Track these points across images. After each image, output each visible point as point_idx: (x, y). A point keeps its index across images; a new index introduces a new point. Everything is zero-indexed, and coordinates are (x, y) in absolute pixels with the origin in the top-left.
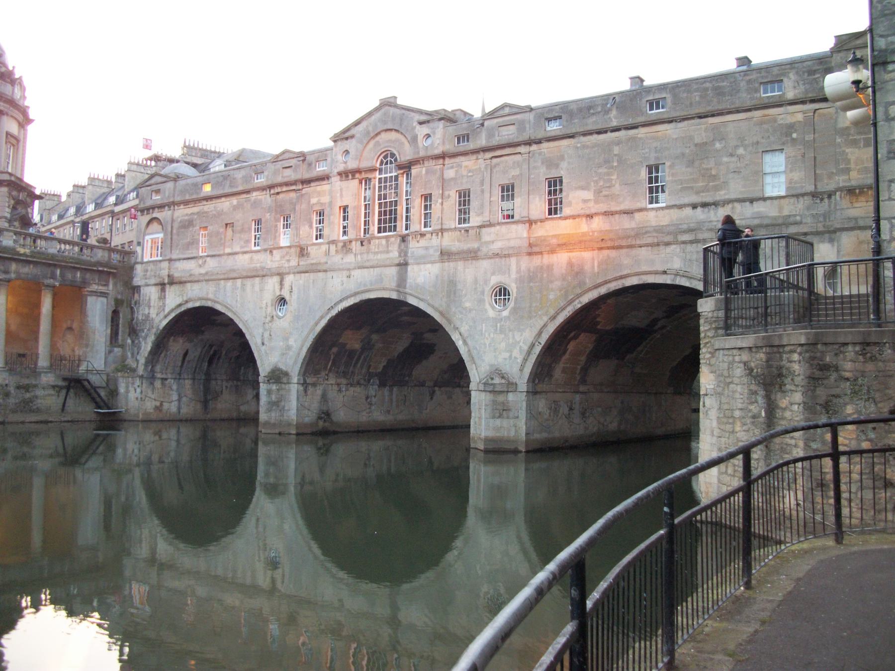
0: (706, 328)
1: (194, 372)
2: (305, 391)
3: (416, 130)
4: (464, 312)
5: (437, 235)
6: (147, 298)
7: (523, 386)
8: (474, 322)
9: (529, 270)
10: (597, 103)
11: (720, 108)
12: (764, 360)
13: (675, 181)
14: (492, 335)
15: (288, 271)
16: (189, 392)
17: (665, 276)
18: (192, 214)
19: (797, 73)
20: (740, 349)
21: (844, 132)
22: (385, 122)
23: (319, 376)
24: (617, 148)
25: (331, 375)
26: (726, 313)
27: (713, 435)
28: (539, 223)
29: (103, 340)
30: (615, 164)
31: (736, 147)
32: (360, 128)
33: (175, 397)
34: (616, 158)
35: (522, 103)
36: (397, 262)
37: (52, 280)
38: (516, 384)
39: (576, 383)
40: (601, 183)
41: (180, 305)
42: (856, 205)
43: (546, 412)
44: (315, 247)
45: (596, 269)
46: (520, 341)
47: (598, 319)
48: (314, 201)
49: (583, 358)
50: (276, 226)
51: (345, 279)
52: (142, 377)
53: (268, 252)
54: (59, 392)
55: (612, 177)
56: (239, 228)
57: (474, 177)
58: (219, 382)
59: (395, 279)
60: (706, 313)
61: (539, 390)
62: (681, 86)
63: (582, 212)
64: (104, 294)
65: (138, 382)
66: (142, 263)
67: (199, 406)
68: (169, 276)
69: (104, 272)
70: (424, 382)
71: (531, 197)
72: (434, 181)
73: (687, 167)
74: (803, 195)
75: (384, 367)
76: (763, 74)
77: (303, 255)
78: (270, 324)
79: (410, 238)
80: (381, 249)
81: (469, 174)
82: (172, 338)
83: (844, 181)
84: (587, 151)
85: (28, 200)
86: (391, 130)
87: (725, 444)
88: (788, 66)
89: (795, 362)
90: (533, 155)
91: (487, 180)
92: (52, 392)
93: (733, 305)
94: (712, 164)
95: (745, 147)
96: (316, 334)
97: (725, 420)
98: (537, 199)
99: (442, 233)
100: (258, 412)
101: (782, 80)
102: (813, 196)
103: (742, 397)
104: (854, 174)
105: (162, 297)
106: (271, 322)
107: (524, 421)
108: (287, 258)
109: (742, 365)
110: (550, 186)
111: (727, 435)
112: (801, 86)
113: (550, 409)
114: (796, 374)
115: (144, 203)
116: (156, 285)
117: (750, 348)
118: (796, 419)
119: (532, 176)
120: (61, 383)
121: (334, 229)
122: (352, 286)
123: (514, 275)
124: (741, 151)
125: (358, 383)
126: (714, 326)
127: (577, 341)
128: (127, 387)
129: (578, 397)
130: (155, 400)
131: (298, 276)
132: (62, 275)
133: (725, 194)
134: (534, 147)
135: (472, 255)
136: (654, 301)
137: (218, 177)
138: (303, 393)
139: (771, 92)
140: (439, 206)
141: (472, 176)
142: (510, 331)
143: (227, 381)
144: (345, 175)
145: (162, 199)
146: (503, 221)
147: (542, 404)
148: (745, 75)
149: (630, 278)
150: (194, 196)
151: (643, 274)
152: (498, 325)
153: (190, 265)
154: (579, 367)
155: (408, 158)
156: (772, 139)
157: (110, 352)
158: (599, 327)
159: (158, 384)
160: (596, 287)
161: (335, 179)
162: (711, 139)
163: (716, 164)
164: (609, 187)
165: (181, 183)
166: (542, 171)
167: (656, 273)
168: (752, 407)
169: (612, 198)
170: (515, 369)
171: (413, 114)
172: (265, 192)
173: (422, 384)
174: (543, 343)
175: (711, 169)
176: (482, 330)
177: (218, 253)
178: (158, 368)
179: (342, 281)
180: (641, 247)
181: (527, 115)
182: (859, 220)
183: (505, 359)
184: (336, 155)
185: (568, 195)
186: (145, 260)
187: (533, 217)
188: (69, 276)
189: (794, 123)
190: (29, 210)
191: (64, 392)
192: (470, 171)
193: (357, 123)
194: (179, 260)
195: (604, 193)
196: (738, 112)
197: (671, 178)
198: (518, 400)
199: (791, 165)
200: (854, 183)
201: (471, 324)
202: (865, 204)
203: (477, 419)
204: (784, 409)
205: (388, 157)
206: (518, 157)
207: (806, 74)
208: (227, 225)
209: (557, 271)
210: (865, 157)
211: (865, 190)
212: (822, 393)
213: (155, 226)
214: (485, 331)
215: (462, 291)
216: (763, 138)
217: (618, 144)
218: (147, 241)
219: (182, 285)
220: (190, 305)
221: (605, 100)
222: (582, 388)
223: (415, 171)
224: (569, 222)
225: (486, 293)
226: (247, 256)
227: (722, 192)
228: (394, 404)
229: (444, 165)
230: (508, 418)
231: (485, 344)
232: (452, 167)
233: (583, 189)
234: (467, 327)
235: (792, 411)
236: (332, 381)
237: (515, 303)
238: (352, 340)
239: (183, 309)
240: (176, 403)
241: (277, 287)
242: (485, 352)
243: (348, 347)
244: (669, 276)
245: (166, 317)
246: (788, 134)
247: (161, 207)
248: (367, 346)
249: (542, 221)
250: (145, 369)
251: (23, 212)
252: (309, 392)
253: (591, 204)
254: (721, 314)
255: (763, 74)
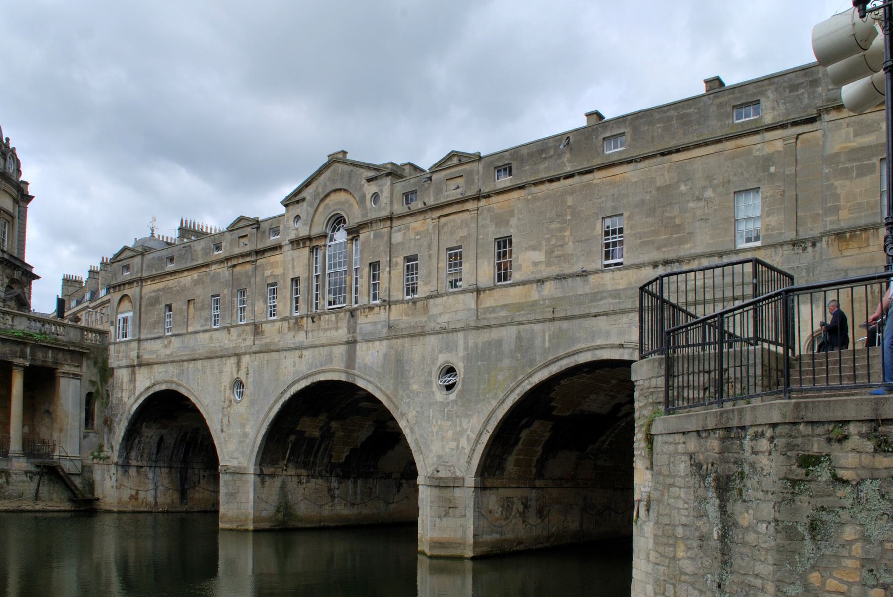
0: (642, 404)
1: (171, 460)
2: (263, 482)
3: (364, 189)
4: (411, 396)
5: (385, 308)
6: (120, 381)
7: (471, 481)
8: (421, 408)
9: (476, 345)
10: (550, 145)
11: (686, 141)
12: (717, 450)
13: (634, 234)
14: (439, 423)
15: (243, 351)
16: (166, 482)
17: (621, 350)
18: (158, 290)
19: (776, 90)
20: (684, 433)
21: (832, 160)
22: (334, 181)
23: (277, 466)
24: (571, 198)
25: (290, 465)
26: (667, 381)
27: (649, 561)
28: (487, 292)
29: (77, 424)
30: (568, 218)
31: (704, 188)
32: (310, 189)
33: (151, 486)
34: (569, 211)
35: (471, 151)
36: (345, 340)
37: (22, 359)
38: (463, 478)
39: (532, 477)
40: (553, 241)
41: (148, 388)
42: (846, 253)
43: (498, 511)
44: (269, 325)
45: (547, 344)
46: (468, 428)
47: (552, 404)
48: (268, 273)
49: (540, 449)
50: (232, 302)
51: (297, 359)
52: (116, 464)
53: (226, 330)
54: (31, 478)
55: (565, 234)
56: (200, 305)
57: (422, 240)
58: (196, 471)
59: (345, 359)
60: (641, 383)
61: (488, 485)
62: (642, 117)
63: (532, 277)
64: (76, 376)
65: (113, 469)
66: (115, 344)
67: (176, 496)
68: (138, 357)
69: (78, 354)
70: (391, 473)
71: (479, 261)
72: (383, 247)
73: (647, 217)
74: (782, 244)
75: (347, 457)
76: (737, 95)
77: (258, 334)
78: (228, 409)
79: (359, 312)
80: (331, 326)
81: (418, 237)
82: (145, 424)
83: (831, 223)
84: (538, 204)
85: (24, 279)
86: (340, 190)
87: (664, 575)
88: (766, 82)
89: (763, 452)
90: (482, 212)
91: (435, 243)
92: (24, 478)
93: (675, 369)
94: (676, 211)
95: (715, 189)
96: (270, 420)
97: (665, 540)
98: (486, 263)
99: (390, 306)
100: (216, 504)
101: (759, 100)
102: (794, 245)
103: (686, 506)
104: (844, 214)
105: (133, 380)
106: (229, 406)
107: (471, 521)
108: (243, 336)
109: (687, 458)
110: (499, 248)
111: (667, 561)
112: (781, 105)
113: (502, 507)
114: (765, 472)
115: (116, 280)
116: (127, 367)
117: (698, 432)
118: (763, 545)
119: (481, 237)
120: (33, 469)
121: (284, 306)
122: (303, 368)
123: (461, 353)
124: (709, 193)
125: (320, 475)
126: (651, 401)
127: (531, 428)
128: (103, 474)
129: (534, 494)
130: (131, 488)
131: (253, 356)
132: (33, 354)
133: (690, 249)
134: (483, 202)
135: (418, 334)
136: (614, 382)
137: (180, 250)
138: (259, 484)
139: (745, 118)
140: (386, 274)
141: (419, 239)
142: (457, 417)
143: (205, 470)
144: (296, 243)
145: (132, 274)
146: (451, 290)
147: (492, 500)
148: (715, 97)
149: (583, 354)
150: (160, 272)
151: (598, 349)
152: (446, 410)
153: (157, 345)
154: (535, 459)
155: (357, 221)
156: (746, 175)
157: (85, 437)
158: (554, 413)
159: (133, 471)
160: (546, 365)
161: (287, 248)
162: (676, 181)
163: (680, 212)
164: (561, 246)
165: (149, 257)
166: (490, 230)
167: (612, 347)
168: (699, 523)
169: (565, 259)
170: (463, 460)
171: (361, 170)
172: (222, 265)
173: (388, 476)
174: (491, 431)
175: (675, 218)
176: (429, 416)
177: (181, 332)
178: (133, 454)
179: (294, 362)
180: (596, 316)
181: (475, 164)
182: (849, 272)
183: (453, 449)
184: (288, 221)
185: (518, 257)
186: (118, 340)
187: (482, 285)
188: (40, 355)
189: (773, 153)
190: (26, 290)
191: (37, 477)
192: (418, 234)
193: (307, 184)
194: (147, 340)
195: (556, 253)
196: (706, 144)
197: (629, 231)
198: (466, 496)
199: (769, 209)
200: (844, 225)
201: (418, 409)
202: (856, 251)
203: (424, 517)
204: (747, 529)
205: (338, 221)
206: (466, 215)
207: (787, 90)
208: (189, 301)
209: (506, 348)
210: (858, 190)
211: (858, 233)
212: (805, 506)
213: (126, 304)
214: (433, 417)
215: (409, 371)
216: (735, 175)
217: (572, 193)
218: (119, 319)
219: (149, 366)
220: (157, 389)
221: (557, 141)
222: (538, 483)
223: (363, 236)
224: (518, 289)
225: (433, 373)
226: (207, 335)
227: (687, 246)
228: (359, 497)
229: (391, 228)
230: (454, 516)
231: (432, 432)
232: (400, 230)
233: (533, 250)
234: (414, 413)
235: (757, 532)
236: (291, 472)
237: (463, 386)
238: (311, 427)
239: (151, 392)
240: (153, 492)
241: (235, 369)
242: (432, 441)
243: (307, 435)
244: (626, 351)
245: (136, 401)
246: (766, 169)
247: (130, 283)
248: (327, 434)
249: (490, 289)
250: (119, 457)
251: (19, 291)
252: (267, 484)
253: (542, 267)
254: (661, 382)
255: (737, 95)
